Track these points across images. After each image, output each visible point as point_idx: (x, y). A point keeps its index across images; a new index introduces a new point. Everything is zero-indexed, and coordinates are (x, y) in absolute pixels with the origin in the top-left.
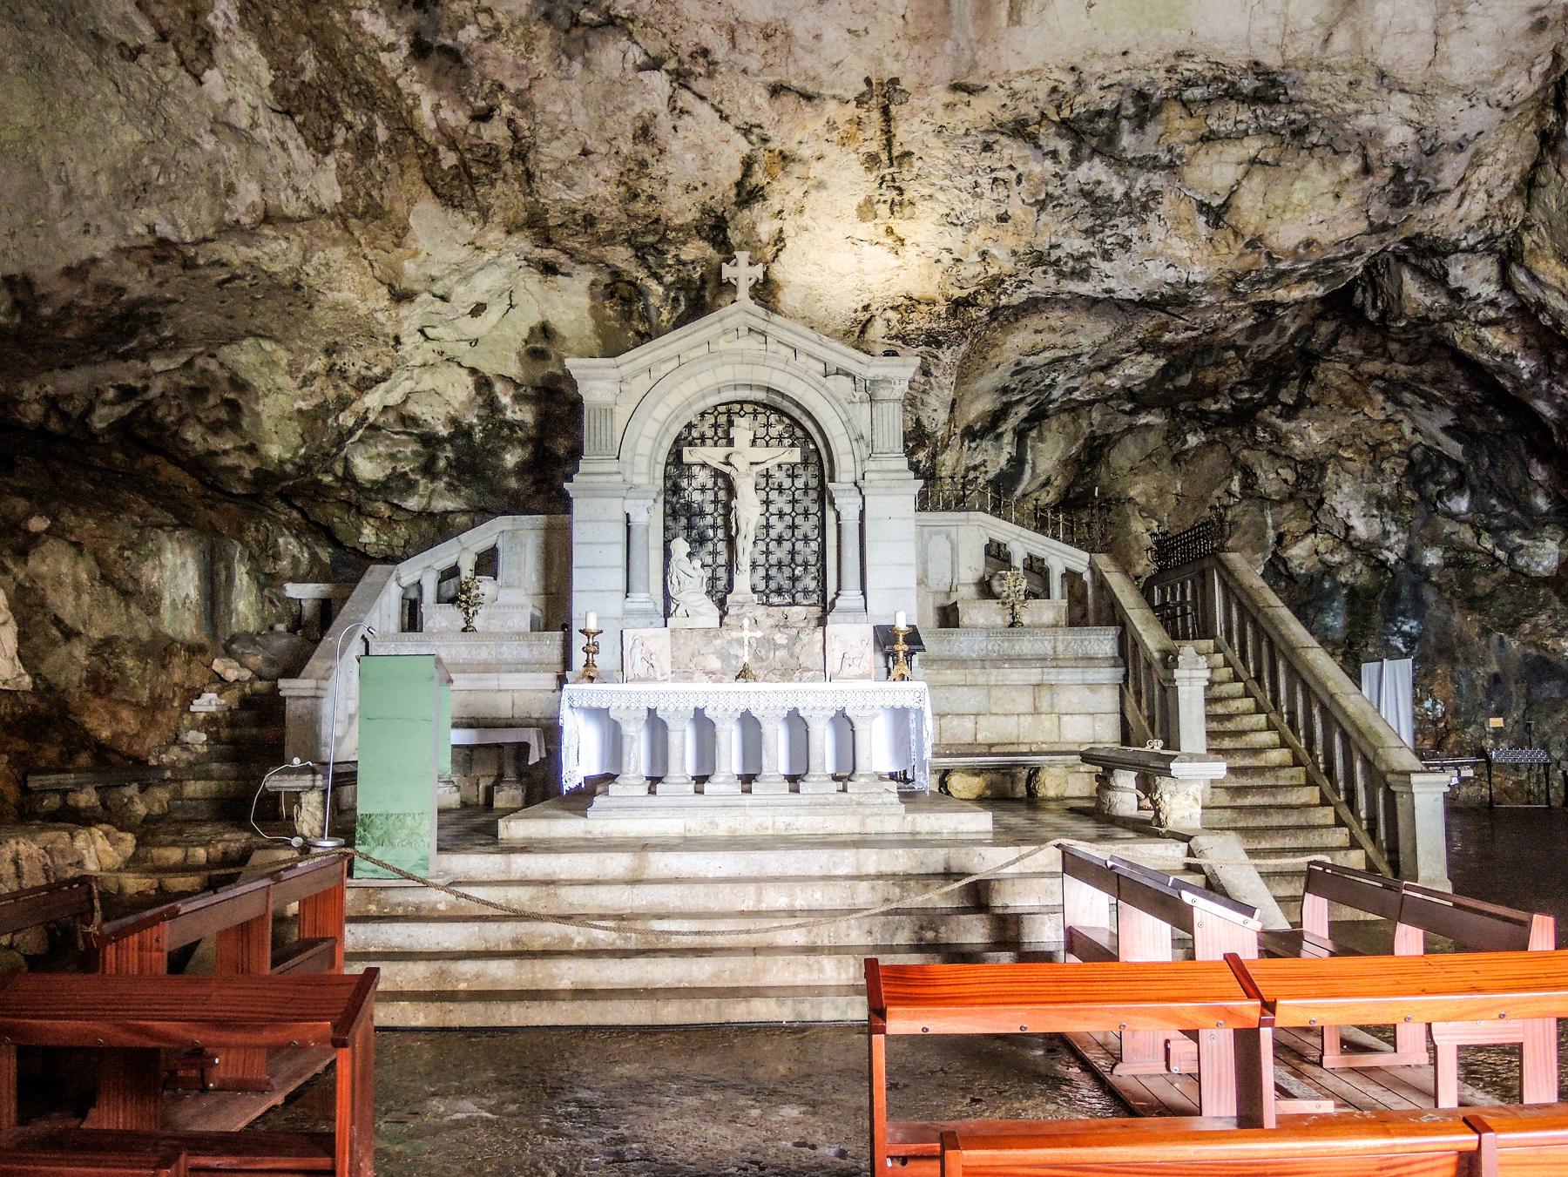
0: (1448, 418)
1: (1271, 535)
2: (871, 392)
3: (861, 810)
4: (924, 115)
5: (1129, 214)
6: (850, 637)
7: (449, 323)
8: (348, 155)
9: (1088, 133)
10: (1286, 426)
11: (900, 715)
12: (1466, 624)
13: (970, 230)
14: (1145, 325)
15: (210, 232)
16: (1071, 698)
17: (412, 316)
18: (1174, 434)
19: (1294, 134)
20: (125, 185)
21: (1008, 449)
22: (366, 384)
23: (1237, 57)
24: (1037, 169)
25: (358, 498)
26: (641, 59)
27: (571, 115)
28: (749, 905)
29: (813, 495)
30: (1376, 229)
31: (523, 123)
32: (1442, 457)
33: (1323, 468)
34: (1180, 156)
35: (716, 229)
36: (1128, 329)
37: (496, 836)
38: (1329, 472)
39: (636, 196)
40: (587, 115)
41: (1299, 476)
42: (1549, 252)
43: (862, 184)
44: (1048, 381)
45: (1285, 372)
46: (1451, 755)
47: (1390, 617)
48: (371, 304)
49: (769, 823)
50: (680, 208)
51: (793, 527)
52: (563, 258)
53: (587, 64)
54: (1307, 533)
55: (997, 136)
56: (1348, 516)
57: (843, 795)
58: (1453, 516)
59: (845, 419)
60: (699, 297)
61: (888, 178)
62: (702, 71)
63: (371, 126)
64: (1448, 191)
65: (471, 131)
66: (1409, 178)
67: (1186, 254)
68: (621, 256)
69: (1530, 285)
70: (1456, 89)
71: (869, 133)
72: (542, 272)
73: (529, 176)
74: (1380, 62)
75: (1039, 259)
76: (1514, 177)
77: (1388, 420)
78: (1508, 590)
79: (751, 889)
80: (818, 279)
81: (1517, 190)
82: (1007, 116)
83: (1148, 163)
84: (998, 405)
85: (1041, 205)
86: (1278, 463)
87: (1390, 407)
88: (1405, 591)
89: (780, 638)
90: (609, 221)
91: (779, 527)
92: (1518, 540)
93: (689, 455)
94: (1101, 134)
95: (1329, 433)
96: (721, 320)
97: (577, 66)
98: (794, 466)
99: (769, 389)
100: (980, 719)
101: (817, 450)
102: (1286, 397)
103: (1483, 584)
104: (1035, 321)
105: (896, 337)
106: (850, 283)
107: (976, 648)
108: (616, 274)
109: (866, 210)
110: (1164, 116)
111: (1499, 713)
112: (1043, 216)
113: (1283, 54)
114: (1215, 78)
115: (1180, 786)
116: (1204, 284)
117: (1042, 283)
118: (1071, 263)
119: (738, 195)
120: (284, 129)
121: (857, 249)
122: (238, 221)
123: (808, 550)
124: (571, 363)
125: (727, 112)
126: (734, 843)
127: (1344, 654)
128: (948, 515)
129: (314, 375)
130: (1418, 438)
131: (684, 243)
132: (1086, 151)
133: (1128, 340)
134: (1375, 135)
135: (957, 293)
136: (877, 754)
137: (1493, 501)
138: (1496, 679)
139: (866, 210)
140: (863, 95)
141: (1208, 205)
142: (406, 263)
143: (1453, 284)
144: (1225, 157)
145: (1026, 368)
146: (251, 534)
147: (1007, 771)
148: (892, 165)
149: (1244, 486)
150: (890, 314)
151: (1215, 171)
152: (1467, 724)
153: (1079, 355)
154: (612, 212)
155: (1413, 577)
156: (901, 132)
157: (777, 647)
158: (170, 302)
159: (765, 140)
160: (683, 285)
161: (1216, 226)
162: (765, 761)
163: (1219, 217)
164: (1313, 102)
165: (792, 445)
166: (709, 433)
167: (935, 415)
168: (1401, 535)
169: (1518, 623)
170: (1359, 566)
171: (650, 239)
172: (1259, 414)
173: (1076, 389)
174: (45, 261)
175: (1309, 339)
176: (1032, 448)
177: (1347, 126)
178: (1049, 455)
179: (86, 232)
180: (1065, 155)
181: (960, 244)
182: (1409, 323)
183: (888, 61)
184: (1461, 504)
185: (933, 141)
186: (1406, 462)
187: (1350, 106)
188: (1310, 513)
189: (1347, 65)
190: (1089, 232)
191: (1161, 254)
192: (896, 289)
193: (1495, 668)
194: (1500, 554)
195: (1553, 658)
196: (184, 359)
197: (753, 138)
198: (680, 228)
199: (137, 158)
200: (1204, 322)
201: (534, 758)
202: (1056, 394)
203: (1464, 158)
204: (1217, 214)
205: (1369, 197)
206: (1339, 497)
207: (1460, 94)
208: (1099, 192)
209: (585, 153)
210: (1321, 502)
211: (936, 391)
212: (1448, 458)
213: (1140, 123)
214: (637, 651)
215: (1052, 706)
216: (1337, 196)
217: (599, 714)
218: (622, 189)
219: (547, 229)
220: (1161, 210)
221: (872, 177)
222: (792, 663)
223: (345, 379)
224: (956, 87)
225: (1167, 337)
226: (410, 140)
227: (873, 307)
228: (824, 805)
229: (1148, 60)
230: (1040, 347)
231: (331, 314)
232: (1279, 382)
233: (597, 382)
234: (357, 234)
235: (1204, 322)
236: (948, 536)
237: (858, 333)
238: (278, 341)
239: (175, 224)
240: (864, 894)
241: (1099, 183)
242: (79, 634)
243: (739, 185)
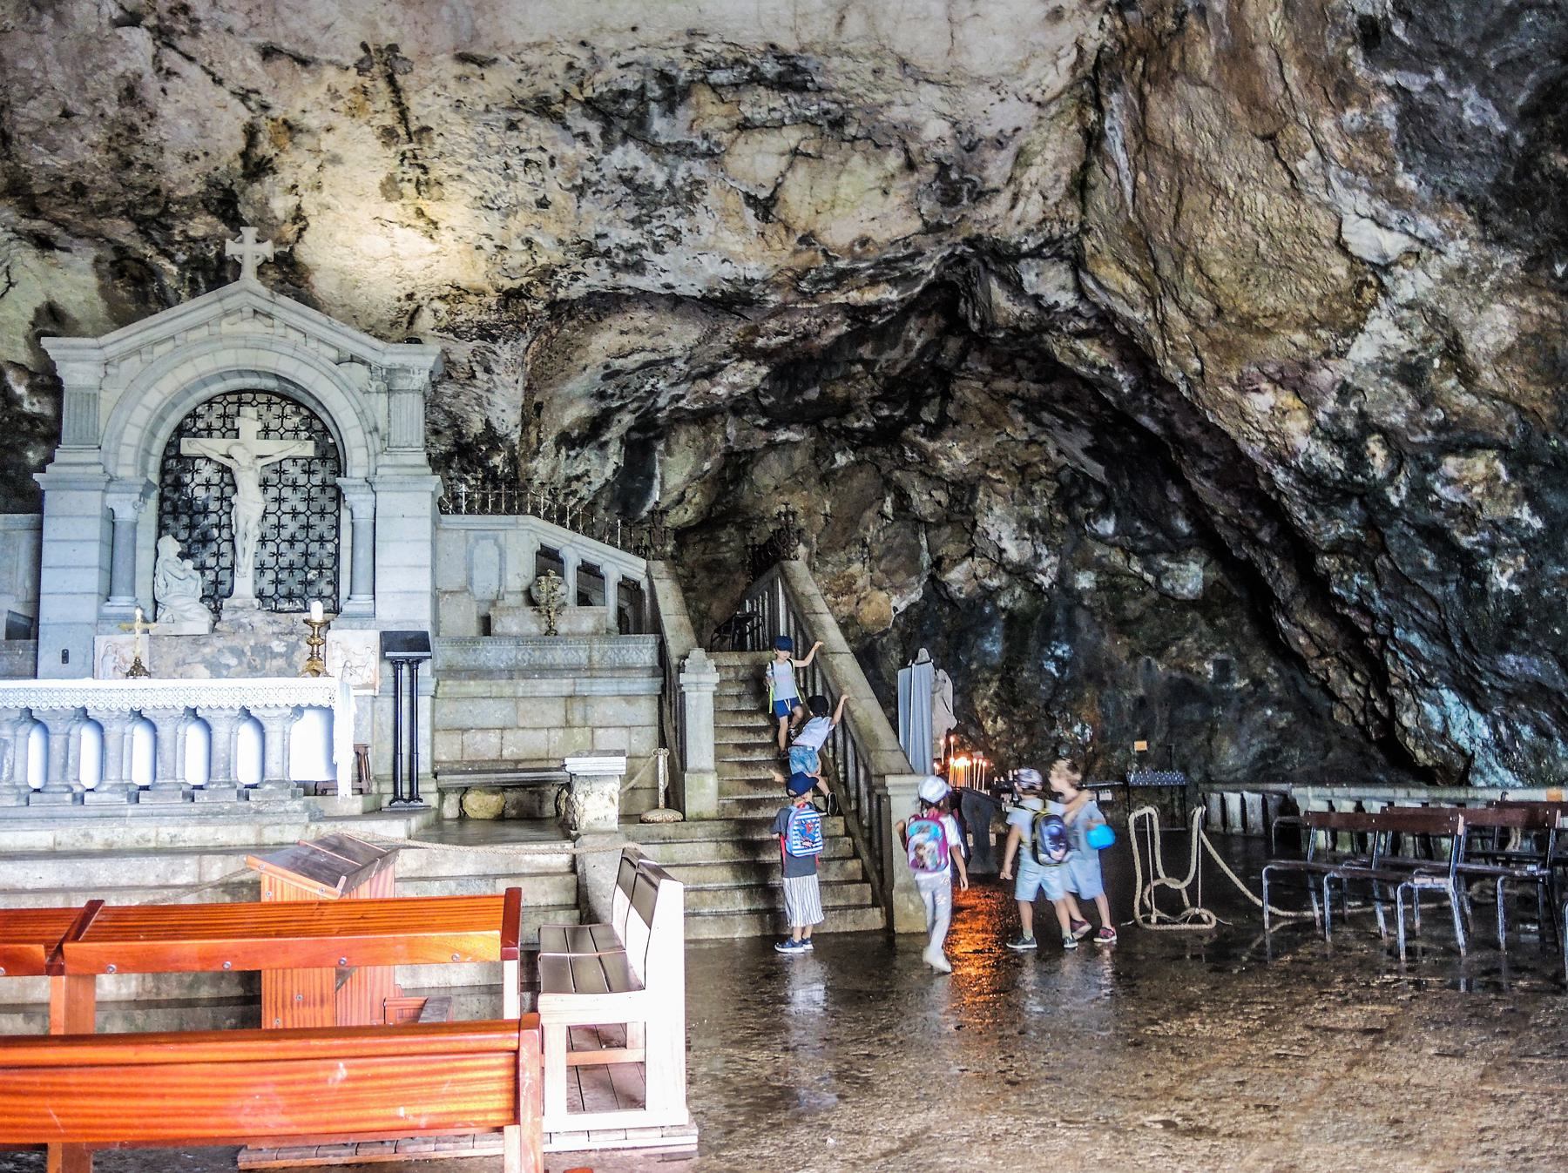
0: (1086, 439)
1: (926, 559)
2: (389, 381)
3: (258, 818)
5: (675, 204)
9: (618, 115)
10: (931, 446)
12: (1115, 647)
13: (507, 216)
16: (604, 711)
18: (820, 454)
21: (615, 457)
23: (752, 39)
24: (570, 152)
26: (117, 14)
27: (46, 73)
30: (933, 228)
32: (1088, 479)
33: (974, 490)
34: (718, 144)
36: (716, 332)
38: (981, 495)
39: (128, 164)
40: (64, 73)
41: (952, 498)
42: (1108, 257)
43: (386, 161)
44: (648, 388)
45: (920, 391)
46: (1098, 779)
47: (1045, 642)
49: (152, 835)
51: (307, 527)
52: (57, 231)
53: (59, 18)
55: (522, 115)
56: (1000, 538)
62: (185, 29)
64: (997, 191)
67: (739, 248)
68: (122, 230)
69: (1099, 292)
70: (980, 81)
72: (36, 246)
74: (898, 49)
75: (589, 251)
76: (1064, 177)
77: (1031, 441)
78: (1157, 613)
81: (1070, 194)
82: (524, 92)
83: (683, 150)
84: (596, 412)
85: (580, 191)
86: (930, 484)
87: (1032, 428)
88: (1059, 617)
90: (103, 191)
91: (292, 527)
92: (1164, 563)
94: (629, 116)
95: (974, 453)
96: (220, 300)
97: (48, 21)
98: (310, 461)
99: (277, 377)
100: (507, 734)
102: (929, 415)
103: (1133, 608)
104: (619, 322)
105: (446, 329)
106: (386, 268)
107: (504, 657)
108: (120, 250)
109: (390, 188)
110: (693, 100)
111: (1143, 737)
112: (583, 203)
113: (798, 37)
114: (737, 61)
116: (764, 281)
117: (597, 277)
118: (622, 255)
119: (245, 166)
121: (394, 233)
123: (324, 553)
125: (219, 75)
127: (1001, 680)
128: (495, 518)
130: (1064, 460)
131: (191, 218)
132: (617, 135)
133: (719, 345)
135: (508, 284)
138: (1141, 702)
139: (390, 188)
140: (362, 61)
141: (755, 197)
143: (1030, 292)
144: (765, 147)
147: (535, 788)
148: (411, 140)
150: (437, 304)
151: (758, 161)
152: (1114, 748)
154: (105, 180)
155: (1067, 601)
156: (413, 102)
157: (274, 655)
161: (765, 219)
164: (842, 91)
165: (310, 438)
166: (217, 424)
167: (503, 416)
168: (1053, 559)
169: (1166, 646)
170: (1018, 591)
171: (150, 212)
172: (905, 433)
173: (683, 397)
175: (937, 355)
176: (661, 462)
177: (881, 117)
180: (596, 137)
181: (499, 230)
182: (1007, 335)
183: (383, 25)
184: (1108, 527)
185: (450, 116)
186: (1056, 485)
187: (881, 97)
189: (866, 52)
190: (636, 222)
191: (713, 248)
192: (439, 276)
193: (1141, 692)
194: (1149, 577)
195: (1197, 681)
197: (252, 104)
198: (183, 201)
200: (793, 326)
202: (662, 402)
203: (1007, 155)
205: (917, 194)
206: (991, 520)
207: (987, 86)
208: (639, 179)
210: (974, 524)
211: (501, 390)
212: (1093, 480)
213: (670, 108)
214: (109, 659)
215: (585, 719)
216: (885, 193)
218: (112, 155)
220: (707, 201)
221: (391, 152)
224: (463, 58)
225: (760, 342)
227: (419, 296)
228: (218, 814)
229: (660, 37)
230: (628, 349)
232: (917, 402)
235: (793, 326)
236: (496, 540)
241: (636, 169)
243: (244, 155)
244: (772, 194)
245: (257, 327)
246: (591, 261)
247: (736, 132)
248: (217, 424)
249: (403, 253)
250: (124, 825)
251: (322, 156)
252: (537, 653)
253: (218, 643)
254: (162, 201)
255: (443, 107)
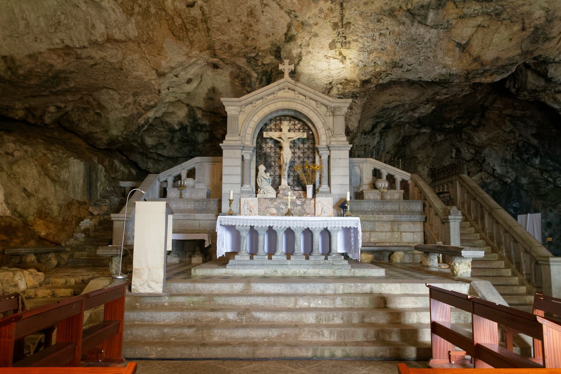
0: (534, 131)
2: (333, 112)
4: (356, 7)
6: (326, 203)
7: (178, 86)
8: (140, 17)
11: (347, 231)
13: (370, 54)
14: (429, 92)
15: (86, 44)
17: (165, 83)
19: (496, 14)
20: (51, 22)
21: (377, 139)
22: (149, 108)
25: (145, 152)
28: (291, 305)
29: (311, 150)
31: (206, 9)
35: (277, 53)
37: (190, 274)
44: (392, 114)
48: (149, 77)
49: (298, 271)
50: (264, 44)
52: (221, 62)
54: (478, 172)
56: (494, 166)
57: (326, 261)
58: (533, 166)
59: (323, 122)
60: (270, 76)
61: (341, 32)
63: (149, 7)
64: (554, 38)
65: (187, 11)
66: (540, 32)
67: (450, 63)
68: (242, 62)
71: (335, 14)
72: (213, 68)
73: (208, 29)
77: (511, 131)
79: (293, 299)
80: (314, 72)
87: (512, 127)
89: (299, 202)
90: (238, 48)
93: (265, 135)
101: (313, 134)
104: (389, 91)
106: (325, 73)
108: (240, 68)
109: (332, 46)
115: (463, 260)
116: (456, 75)
119: (285, 38)
120: (114, 4)
122: (96, 40)
124: (222, 99)
125: (282, 5)
126: (284, 279)
129: (129, 104)
133: (423, 99)
134: (529, 14)
135: (363, 78)
136: (339, 246)
137: (549, 161)
139: (332, 46)
141: (460, 44)
142: (162, 62)
145: (385, 109)
146: (106, 163)
147: (380, 252)
148: (343, 27)
149: (456, 155)
150: (339, 86)
153: (405, 104)
154: (239, 44)
156: (347, 14)
157: (298, 205)
158: (72, 72)
159: (296, 17)
160: (265, 73)
162: (296, 247)
163: (464, 48)
165: (304, 132)
166: (273, 127)
168: (513, 173)
170: (497, 183)
171: (253, 55)
174: (19, 50)
177: (518, 11)
178: (391, 141)
179: (36, 41)
184: (537, 161)
185: (358, 18)
188: (479, 165)
194: (550, 179)
196: (80, 96)
197: (292, 16)
199: (55, 11)
201: (207, 245)
204: (463, 47)
205: (523, 40)
209: (229, 21)
215: (398, 229)
217: (230, 228)
218: (243, 35)
219: (215, 50)
221: (335, 32)
222: (303, 211)
223: (140, 106)
225: (438, 97)
226: (164, 13)
227: (333, 83)
230: (391, 101)
231: (135, 80)
233: (232, 107)
234: (144, 49)
237: (328, 90)
238: (115, 90)
239: (71, 40)
240: (339, 303)
242: (34, 196)
243: (286, 34)
244: (467, 43)
245: (291, 94)
246: (395, 69)
247: (459, 19)
248: (273, 127)
249: (332, 68)
250: (288, 268)
251: (312, 34)
252: (381, 206)
253: (279, 201)
254: (257, 51)
255: (356, 14)
